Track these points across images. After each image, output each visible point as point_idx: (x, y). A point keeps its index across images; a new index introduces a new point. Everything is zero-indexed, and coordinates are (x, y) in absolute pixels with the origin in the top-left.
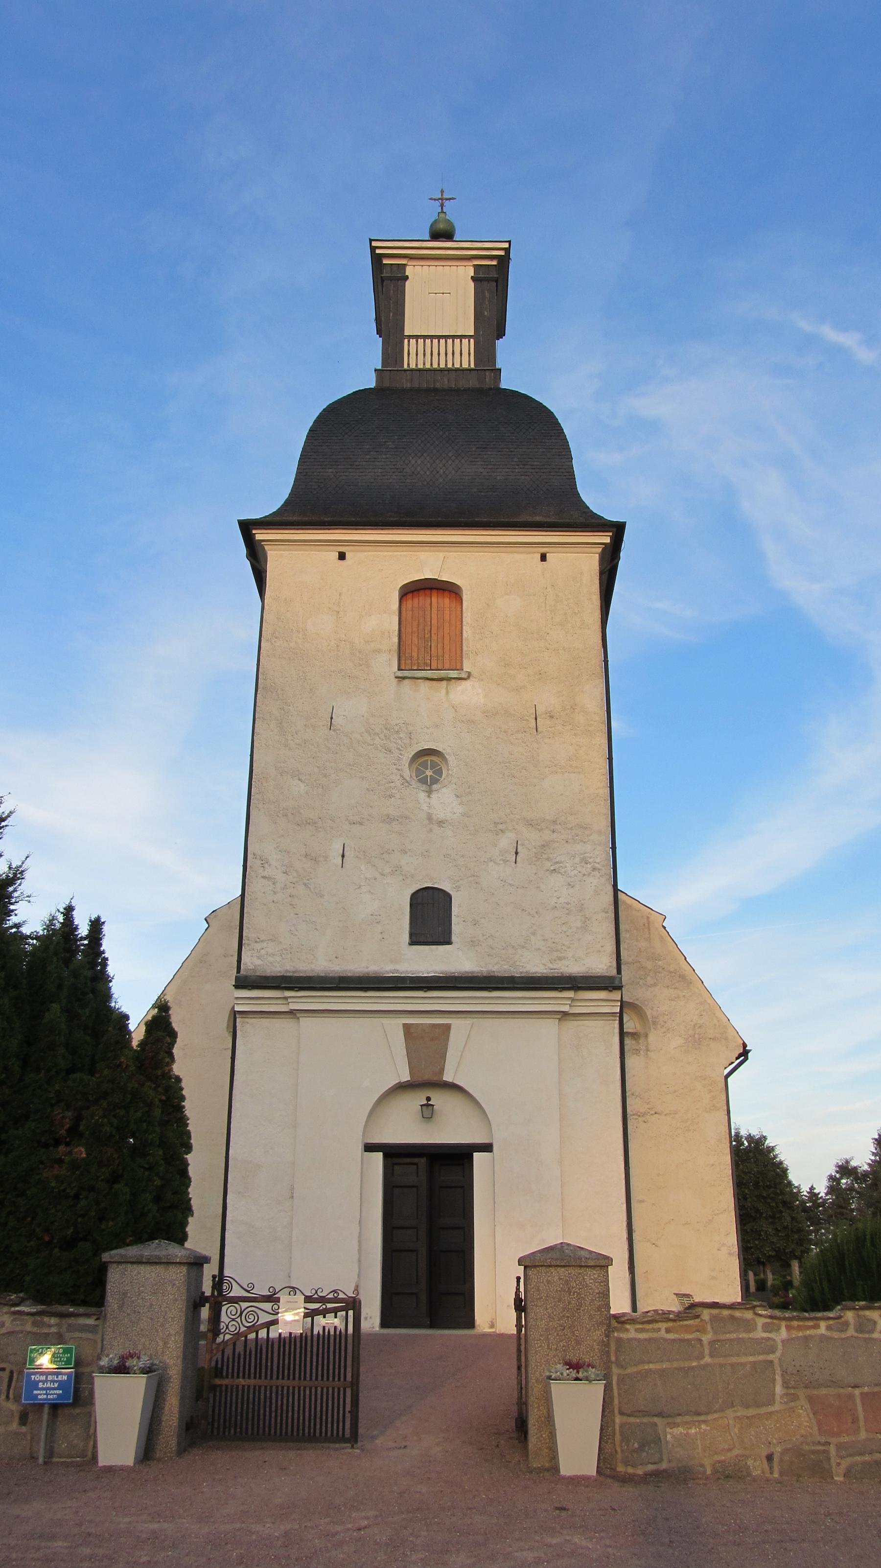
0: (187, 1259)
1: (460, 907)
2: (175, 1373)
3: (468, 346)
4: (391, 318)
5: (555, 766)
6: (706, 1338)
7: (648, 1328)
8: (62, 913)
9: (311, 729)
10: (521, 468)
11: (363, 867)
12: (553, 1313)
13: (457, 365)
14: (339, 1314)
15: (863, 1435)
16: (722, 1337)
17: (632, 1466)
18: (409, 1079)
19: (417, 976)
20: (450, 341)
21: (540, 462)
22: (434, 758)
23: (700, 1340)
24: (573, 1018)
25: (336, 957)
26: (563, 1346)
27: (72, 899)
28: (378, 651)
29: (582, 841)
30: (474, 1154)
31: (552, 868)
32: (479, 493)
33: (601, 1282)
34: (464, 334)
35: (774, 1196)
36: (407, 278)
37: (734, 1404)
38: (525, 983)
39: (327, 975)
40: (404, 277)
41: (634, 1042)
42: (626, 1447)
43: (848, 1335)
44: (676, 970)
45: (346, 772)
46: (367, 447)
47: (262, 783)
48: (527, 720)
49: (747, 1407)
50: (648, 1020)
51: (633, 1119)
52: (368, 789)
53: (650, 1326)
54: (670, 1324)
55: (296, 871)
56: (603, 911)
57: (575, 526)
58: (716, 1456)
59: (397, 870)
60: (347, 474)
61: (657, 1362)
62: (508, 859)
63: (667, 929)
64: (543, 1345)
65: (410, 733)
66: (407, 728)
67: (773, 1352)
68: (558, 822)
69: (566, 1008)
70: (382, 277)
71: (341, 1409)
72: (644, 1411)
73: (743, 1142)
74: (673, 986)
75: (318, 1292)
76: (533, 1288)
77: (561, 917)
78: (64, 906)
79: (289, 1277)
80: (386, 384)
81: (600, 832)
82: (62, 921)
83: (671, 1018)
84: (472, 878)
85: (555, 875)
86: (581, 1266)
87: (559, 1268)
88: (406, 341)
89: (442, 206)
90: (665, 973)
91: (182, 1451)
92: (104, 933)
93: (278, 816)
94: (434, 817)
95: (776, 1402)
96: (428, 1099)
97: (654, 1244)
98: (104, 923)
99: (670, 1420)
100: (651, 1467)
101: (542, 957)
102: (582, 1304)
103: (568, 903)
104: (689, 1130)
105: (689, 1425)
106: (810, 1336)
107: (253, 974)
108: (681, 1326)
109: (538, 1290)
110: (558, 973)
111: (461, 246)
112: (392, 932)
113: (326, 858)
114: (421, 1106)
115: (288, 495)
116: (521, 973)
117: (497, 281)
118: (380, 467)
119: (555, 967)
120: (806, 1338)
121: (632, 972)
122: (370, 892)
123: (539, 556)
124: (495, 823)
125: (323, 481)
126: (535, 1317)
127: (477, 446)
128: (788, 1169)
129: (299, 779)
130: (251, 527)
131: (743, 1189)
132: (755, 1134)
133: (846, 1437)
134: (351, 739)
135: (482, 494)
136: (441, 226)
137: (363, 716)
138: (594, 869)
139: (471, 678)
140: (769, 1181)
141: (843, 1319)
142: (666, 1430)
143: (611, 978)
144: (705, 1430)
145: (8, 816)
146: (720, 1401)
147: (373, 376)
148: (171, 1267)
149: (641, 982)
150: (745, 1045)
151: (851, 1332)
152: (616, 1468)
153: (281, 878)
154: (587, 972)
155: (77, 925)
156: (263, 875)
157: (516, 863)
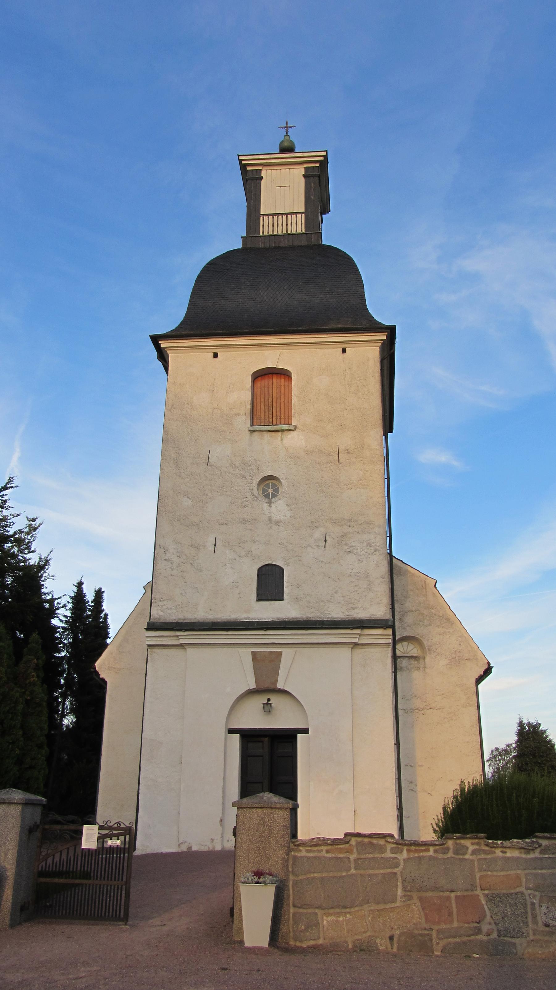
0: (21, 800)
1: (289, 576)
2: (11, 874)
3: (301, 219)
4: (252, 203)
5: (351, 484)
6: (353, 857)
7: (314, 849)
8: (76, 586)
9: (196, 465)
10: (331, 294)
11: (227, 552)
12: (252, 838)
13: (294, 231)
14: (120, 837)
15: (455, 924)
16: (363, 857)
17: (300, 941)
18: (255, 687)
19: (261, 621)
20: (289, 216)
21: (343, 290)
22: (274, 482)
23: (349, 858)
24: (361, 647)
25: (210, 610)
26: (258, 861)
27: (82, 577)
28: (238, 414)
29: (368, 532)
30: (298, 735)
31: (348, 550)
32: (304, 312)
33: (285, 819)
34: (298, 211)
35: (545, 762)
36: (262, 178)
37: (370, 901)
38: (329, 625)
39: (205, 621)
40: (260, 177)
41: (416, 662)
42: (296, 928)
43: (448, 856)
44: (443, 615)
45: (217, 492)
46: (233, 285)
47: (165, 501)
48: (333, 455)
49: (378, 903)
50: (425, 649)
51: (416, 712)
52: (231, 503)
53: (315, 849)
54: (329, 847)
55: (186, 555)
56: (381, 577)
57: (363, 329)
58: (356, 936)
59: (249, 553)
60: (220, 303)
61: (319, 872)
62: (320, 545)
63: (437, 588)
64: (245, 859)
65: (258, 466)
66: (256, 463)
67: (397, 867)
68: (352, 521)
69: (356, 641)
70: (246, 179)
71: (119, 901)
72: (309, 905)
73: (525, 727)
74: (442, 626)
75: (108, 823)
76: (240, 822)
77: (354, 582)
78: (77, 582)
79: (179, 814)
80: (249, 246)
81: (379, 526)
82: (76, 591)
83: (440, 647)
84: (297, 558)
85: (350, 554)
86: (272, 808)
87: (258, 809)
88: (261, 218)
89: (287, 131)
90: (436, 617)
91: (14, 924)
92: (104, 598)
93: (174, 521)
94: (273, 519)
95: (398, 900)
96: (269, 700)
97: (429, 794)
98: (104, 592)
99: (326, 911)
100: (312, 943)
101: (341, 608)
102: (271, 833)
103: (358, 573)
104: (452, 720)
105: (338, 914)
106: (423, 857)
107: (158, 621)
108: (337, 848)
109: (244, 823)
110: (352, 618)
111: (296, 156)
112: (246, 593)
113: (204, 546)
114: (263, 704)
115: (183, 318)
116: (328, 618)
117: (319, 177)
118: (241, 298)
119: (350, 614)
120: (420, 858)
121: (414, 617)
122: (232, 568)
123: (341, 350)
124: (312, 522)
125: (205, 308)
126: (241, 841)
127: (303, 282)
128: (555, 745)
129: (188, 497)
130: (158, 339)
131: (525, 758)
132: (533, 722)
133: (444, 926)
134: (221, 471)
135: (306, 312)
136: (286, 144)
137: (228, 456)
138: (376, 550)
139: (297, 430)
140: (543, 753)
141: (446, 846)
142: (323, 918)
143: (387, 621)
144: (349, 919)
145: (39, 526)
146: (360, 899)
147: (241, 241)
148: (12, 806)
149: (421, 623)
150: (489, 664)
151: (450, 854)
152: (289, 943)
153: (176, 560)
154: (371, 617)
155: (85, 594)
156: (165, 558)
157: (325, 547)
